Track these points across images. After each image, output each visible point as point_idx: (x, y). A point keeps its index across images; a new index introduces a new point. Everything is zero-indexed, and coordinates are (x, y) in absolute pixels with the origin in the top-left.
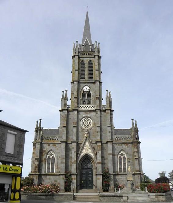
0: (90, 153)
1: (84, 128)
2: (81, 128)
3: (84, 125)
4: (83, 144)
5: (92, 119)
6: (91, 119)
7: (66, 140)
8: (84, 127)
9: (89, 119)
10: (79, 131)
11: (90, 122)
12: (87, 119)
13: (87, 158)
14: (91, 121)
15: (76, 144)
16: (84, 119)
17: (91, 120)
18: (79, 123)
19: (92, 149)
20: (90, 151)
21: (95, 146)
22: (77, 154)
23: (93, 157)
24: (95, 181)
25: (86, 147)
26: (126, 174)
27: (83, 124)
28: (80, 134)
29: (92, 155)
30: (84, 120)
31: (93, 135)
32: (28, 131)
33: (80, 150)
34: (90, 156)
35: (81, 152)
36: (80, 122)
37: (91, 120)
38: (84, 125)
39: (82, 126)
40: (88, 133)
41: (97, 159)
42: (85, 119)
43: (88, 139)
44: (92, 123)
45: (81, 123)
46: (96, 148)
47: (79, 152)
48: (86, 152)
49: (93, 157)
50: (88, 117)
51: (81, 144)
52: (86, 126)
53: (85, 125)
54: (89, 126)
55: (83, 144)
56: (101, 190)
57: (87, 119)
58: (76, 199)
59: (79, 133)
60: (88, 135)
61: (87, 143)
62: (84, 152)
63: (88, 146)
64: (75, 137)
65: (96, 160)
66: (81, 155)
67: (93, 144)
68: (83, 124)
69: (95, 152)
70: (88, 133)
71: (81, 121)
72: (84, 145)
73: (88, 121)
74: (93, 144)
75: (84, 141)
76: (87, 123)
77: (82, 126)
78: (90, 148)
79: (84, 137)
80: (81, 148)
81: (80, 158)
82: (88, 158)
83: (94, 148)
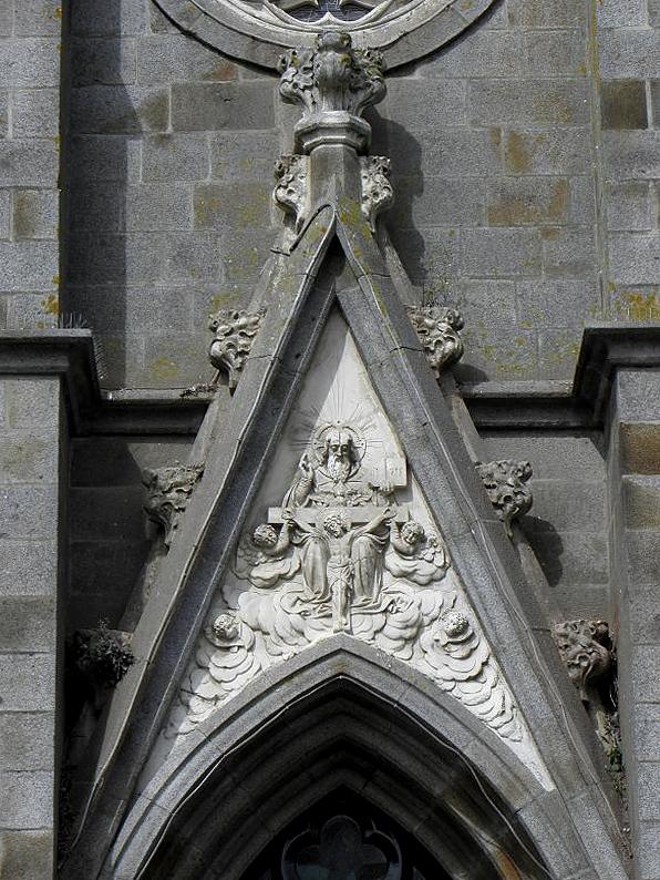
0: (433, 663)
4: (229, 419)
7: (72, 301)
10: (138, 93)
13: (343, 800)
15: (48, 424)
19: (482, 562)
20: (441, 601)
21: (564, 467)
22: (84, 684)
23: (526, 752)
25: (319, 505)
26: (183, 510)
28: (160, 186)
29: (490, 705)
31: (509, 207)
32: (232, 395)
33: (165, 579)
34: (441, 753)
35: (194, 632)
40: (377, 139)
41: (620, 798)
43: (361, 294)
46: (584, 541)
47: (142, 640)
48: (320, 634)
49: (526, 752)
51: (179, 419)
55: (229, 419)
59: (138, 152)
60: (373, 184)
61: (348, 400)
62: (265, 643)
63: (383, 458)
64: (23, 226)
65: (594, 831)
66: (200, 712)
67: (501, 415)
69: (581, 647)
70: (377, 139)
72: (254, 454)
74: (501, 415)
75: (266, 346)
78: (417, 514)
79: (248, 264)
80: (186, 535)
81: (170, 782)
82: (366, 812)
83: (530, 533)
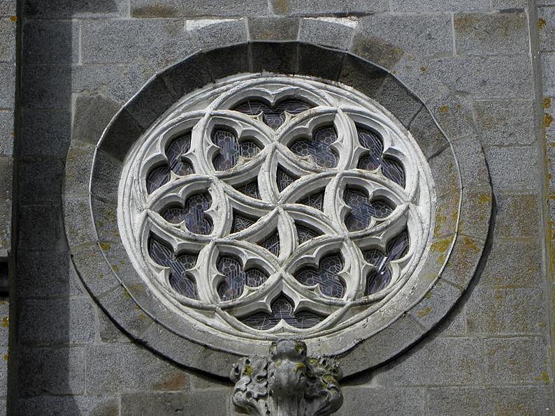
1: (219, 328)
2: (132, 329)
3: (204, 271)
5: (433, 92)
6: (403, 102)
8: (199, 314)
9: (338, 101)
11: (375, 180)
12: (292, 102)
14: (394, 165)
16: (203, 106)
17: (397, 138)
18: (78, 195)
24: (292, 80)
27: (178, 233)
30: (220, 130)
36: (105, 178)
37: (397, 138)
38: (204, 271)
39: (151, 275)
42: (246, 123)
44: (418, 198)
45: (134, 209)
50: (325, 63)
52: (278, 272)
53: (225, 257)
54: (353, 267)
56: (358, 366)
57: (292, 102)
58: (313, 105)
68: (178, 233)
71: (118, 143)
73: (306, 168)
76: (276, 199)
77: (167, 299)
